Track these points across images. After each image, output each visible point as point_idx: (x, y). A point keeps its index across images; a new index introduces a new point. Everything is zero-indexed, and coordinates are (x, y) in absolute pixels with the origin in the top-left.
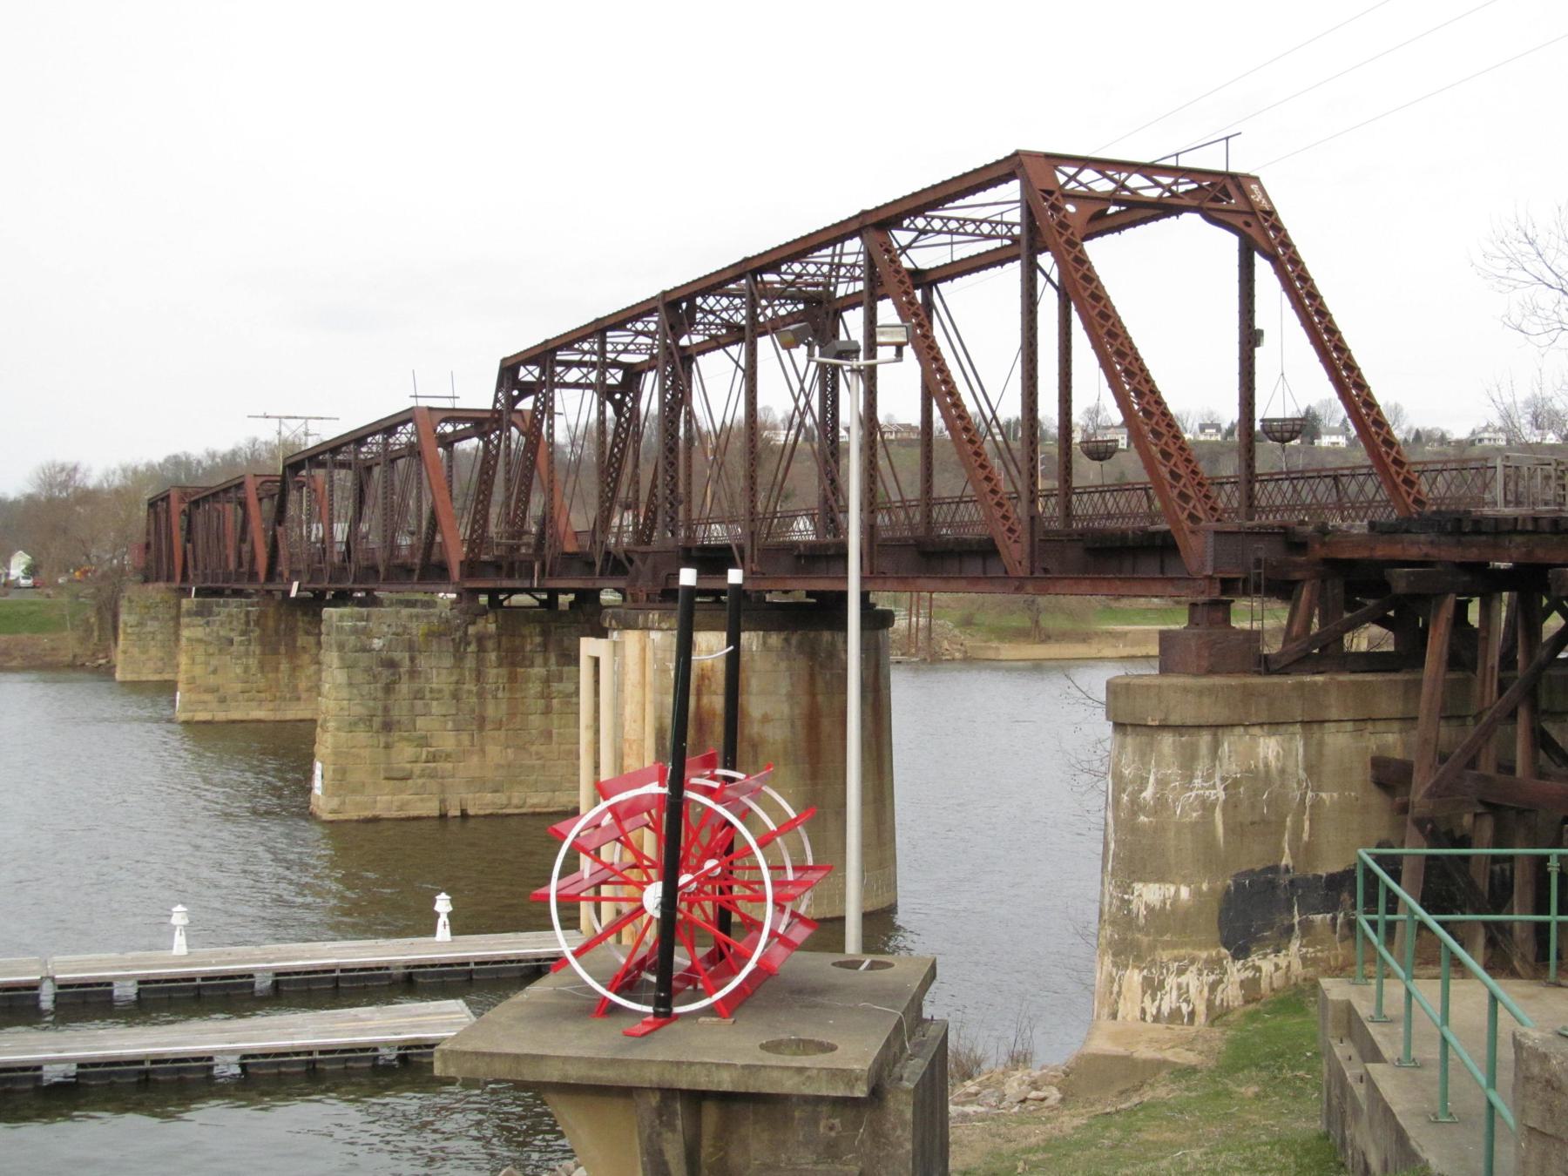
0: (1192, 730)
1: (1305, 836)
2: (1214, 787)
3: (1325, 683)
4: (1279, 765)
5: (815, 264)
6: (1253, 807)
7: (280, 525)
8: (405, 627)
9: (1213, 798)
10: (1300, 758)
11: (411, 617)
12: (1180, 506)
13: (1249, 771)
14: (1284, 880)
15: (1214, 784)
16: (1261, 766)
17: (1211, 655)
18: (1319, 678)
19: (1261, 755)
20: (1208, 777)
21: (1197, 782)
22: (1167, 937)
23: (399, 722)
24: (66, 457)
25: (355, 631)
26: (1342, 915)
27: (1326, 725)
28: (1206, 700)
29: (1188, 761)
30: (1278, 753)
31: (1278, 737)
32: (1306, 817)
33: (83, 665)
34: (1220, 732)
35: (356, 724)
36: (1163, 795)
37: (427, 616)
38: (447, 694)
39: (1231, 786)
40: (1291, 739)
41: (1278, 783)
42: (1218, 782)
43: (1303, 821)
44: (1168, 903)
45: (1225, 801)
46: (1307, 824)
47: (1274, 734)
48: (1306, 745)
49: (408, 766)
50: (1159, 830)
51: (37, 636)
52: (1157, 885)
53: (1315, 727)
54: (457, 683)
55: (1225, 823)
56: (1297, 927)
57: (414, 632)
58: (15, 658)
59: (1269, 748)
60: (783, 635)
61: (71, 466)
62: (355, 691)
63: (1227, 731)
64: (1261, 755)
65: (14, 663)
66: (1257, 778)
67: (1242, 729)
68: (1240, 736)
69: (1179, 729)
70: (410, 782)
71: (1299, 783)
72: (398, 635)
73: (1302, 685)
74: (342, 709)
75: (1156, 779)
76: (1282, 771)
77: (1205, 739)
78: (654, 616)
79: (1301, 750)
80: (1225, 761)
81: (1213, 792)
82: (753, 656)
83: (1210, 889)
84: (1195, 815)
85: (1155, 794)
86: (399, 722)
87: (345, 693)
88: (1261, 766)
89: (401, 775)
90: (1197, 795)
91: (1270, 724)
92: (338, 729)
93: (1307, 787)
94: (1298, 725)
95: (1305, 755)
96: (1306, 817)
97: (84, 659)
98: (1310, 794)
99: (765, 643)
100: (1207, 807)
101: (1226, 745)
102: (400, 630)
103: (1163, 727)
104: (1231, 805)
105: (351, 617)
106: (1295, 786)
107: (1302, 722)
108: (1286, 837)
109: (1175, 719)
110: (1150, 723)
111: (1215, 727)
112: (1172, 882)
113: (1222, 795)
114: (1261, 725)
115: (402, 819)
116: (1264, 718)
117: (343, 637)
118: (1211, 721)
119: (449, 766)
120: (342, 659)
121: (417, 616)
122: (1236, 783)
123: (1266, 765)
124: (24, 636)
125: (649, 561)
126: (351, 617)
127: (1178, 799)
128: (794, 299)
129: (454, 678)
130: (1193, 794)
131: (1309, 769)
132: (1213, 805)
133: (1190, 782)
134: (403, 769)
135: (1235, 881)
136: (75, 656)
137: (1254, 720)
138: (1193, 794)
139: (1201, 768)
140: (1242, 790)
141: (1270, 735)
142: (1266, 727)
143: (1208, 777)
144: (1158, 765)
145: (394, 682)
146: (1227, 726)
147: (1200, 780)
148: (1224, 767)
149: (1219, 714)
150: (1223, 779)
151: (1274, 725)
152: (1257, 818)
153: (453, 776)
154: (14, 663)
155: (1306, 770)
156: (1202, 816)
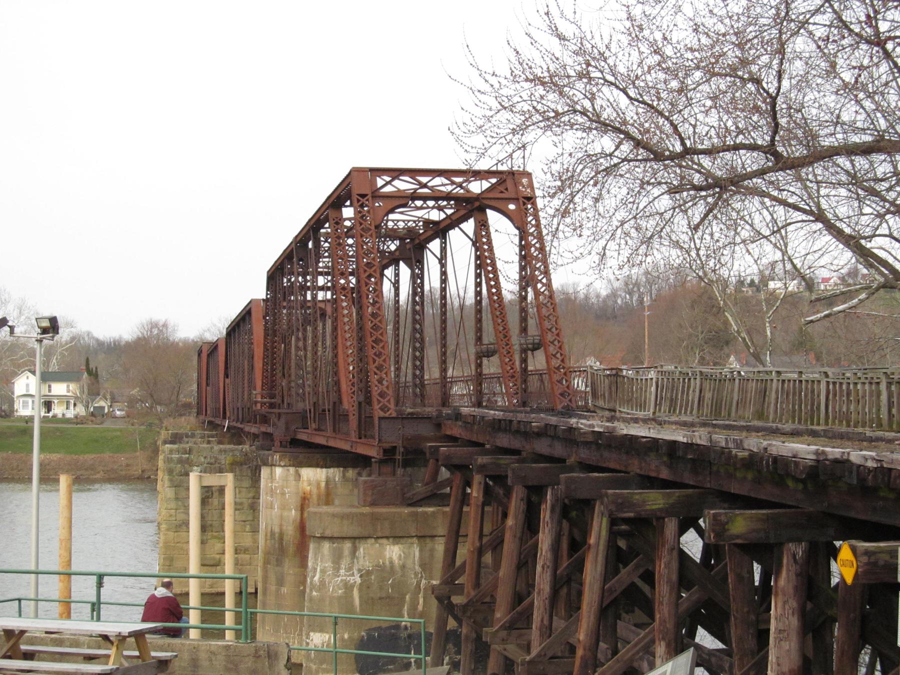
0: (339, 540)
1: (420, 608)
2: (353, 575)
3: (433, 512)
4: (401, 562)
5: (393, 221)
6: (381, 588)
7: (227, 377)
8: (216, 459)
9: (352, 581)
10: (417, 559)
11: (220, 451)
12: (378, 400)
13: (378, 566)
14: (404, 635)
15: (353, 573)
16: (387, 563)
17: (373, 494)
18: (431, 509)
19: (388, 556)
20: (350, 569)
21: (342, 572)
22: (324, 666)
23: (211, 525)
24: (159, 316)
25: (180, 461)
26: (447, 658)
27: (437, 538)
28: (345, 522)
29: (337, 559)
30: (400, 555)
31: (400, 546)
32: (421, 595)
33: (150, 477)
34: (357, 541)
35: (180, 526)
36: (323, 579)
37: (232, 451)
38: (246, 506)
39: (365, 575)
40: (409, 547)
41: (400, 574)
42: (356, 572)
43: (418, 597)
44: (325, 644)
45: (360, 584)
46: (421, 601)
47: (397, 544)
48: (421, 551)
49: (218, 556)
50: (322, 600)
51: (116, 455)
52: (320, 634)
53: (428, 540)
54: (254, 498)
55: (360, 597)
56: (413, 664)
57: (223, 462)
58: (99, 472)
59: (393, 552)
60: (356, 471)
61: (161, 323)
62: (180, 503)
63: (363, 541)
64: (388, 556)
65: (98, 476)
66: (385, 571)
67: (373, 540)
68: (372, 544)
69: (331, 539)
70: (218, 567)
71: (416, 574)
72: (211, 464)
73: (416, 514)
74: (171, 516)
75: (321, 570)
76: (403, 567)
77: (347, 546)
78: (277, 457)
79: (417, 554)
80: (361, 561)
81: (352, 578)
82: (336, 484)
83: (350, 637)
84: (340, 591)
85: (320, 578)
86: (211, 525)
87: (173, 505)
88: (387, 563)
89: (212, 563)
90: (342, 580)
91: (395, 537)
92: (168, 530)
93: (422, 577)
94: (415, 539)
95: (421, 558)
96: (421, 595)
97: (149, 473)
98: (423, 581)
99: (344, 476)
100: (348, 587)
101: (362, 550)
102: (213, 461)
103: (323, 538)
104: (365, 586)
105: (178, 451)
106: (413, 576)
107: (420, 537)
108: (406, 608)
109: (328, 533)
110: (317, 535)
111: (354, 539)
112: (327, 632)
113: (359, 580)
114: (387, 538)
115: (212, 594)
116: (387, 534)
117: (172, 465)
118: (349, 535)
119: (247, 556)
120: (171, 480)
121: (225, 451)
122: (369, 573)
123: (391, 562)
124: (107, 455)
125: (283, 420)
126: (178, 451)
127: (331, 582)
128: (747, 188)
129: (251, 495)
130: (340, 579)
131: (423, 565)
132: (352, 586)
133: (338, 571)
134: (214, 559)
135: (367, 634)
136: (143, 471)
137: (380, 534)
138: (340, 579)
139: (344, 564)
140: (373, 577)
141: (394, 544)
142: (391, 540)
143: (350, 569)
144: (321, 561)
145: (208, 497)
146: (362, 538)
147: (344, 571)
148: (360, 563)
149: (355, 531)
150: (359, 570)
151: (396, 538)
152: (384, 595)
153: (250, 564)
154: (98, 476)
155: (420, 566)
156: (345, 593)
